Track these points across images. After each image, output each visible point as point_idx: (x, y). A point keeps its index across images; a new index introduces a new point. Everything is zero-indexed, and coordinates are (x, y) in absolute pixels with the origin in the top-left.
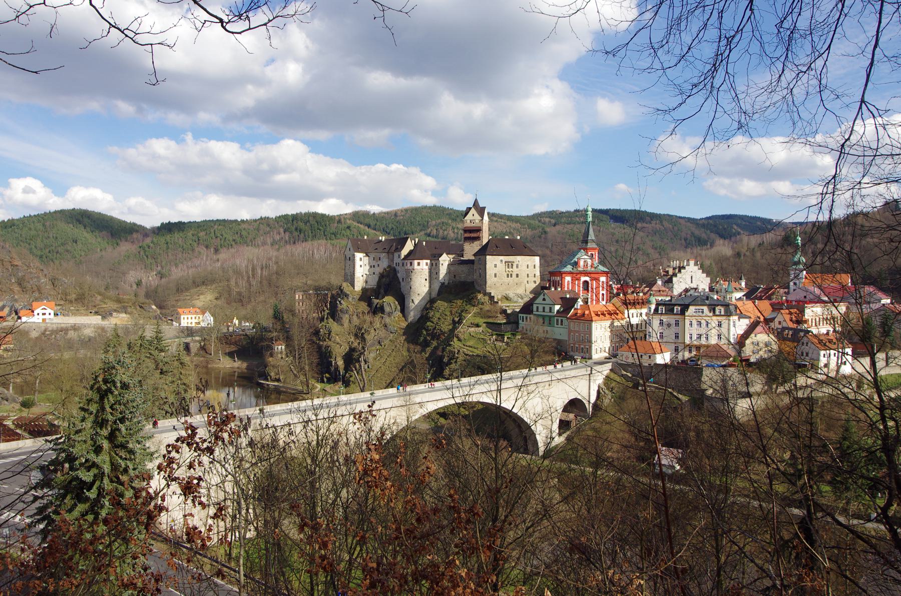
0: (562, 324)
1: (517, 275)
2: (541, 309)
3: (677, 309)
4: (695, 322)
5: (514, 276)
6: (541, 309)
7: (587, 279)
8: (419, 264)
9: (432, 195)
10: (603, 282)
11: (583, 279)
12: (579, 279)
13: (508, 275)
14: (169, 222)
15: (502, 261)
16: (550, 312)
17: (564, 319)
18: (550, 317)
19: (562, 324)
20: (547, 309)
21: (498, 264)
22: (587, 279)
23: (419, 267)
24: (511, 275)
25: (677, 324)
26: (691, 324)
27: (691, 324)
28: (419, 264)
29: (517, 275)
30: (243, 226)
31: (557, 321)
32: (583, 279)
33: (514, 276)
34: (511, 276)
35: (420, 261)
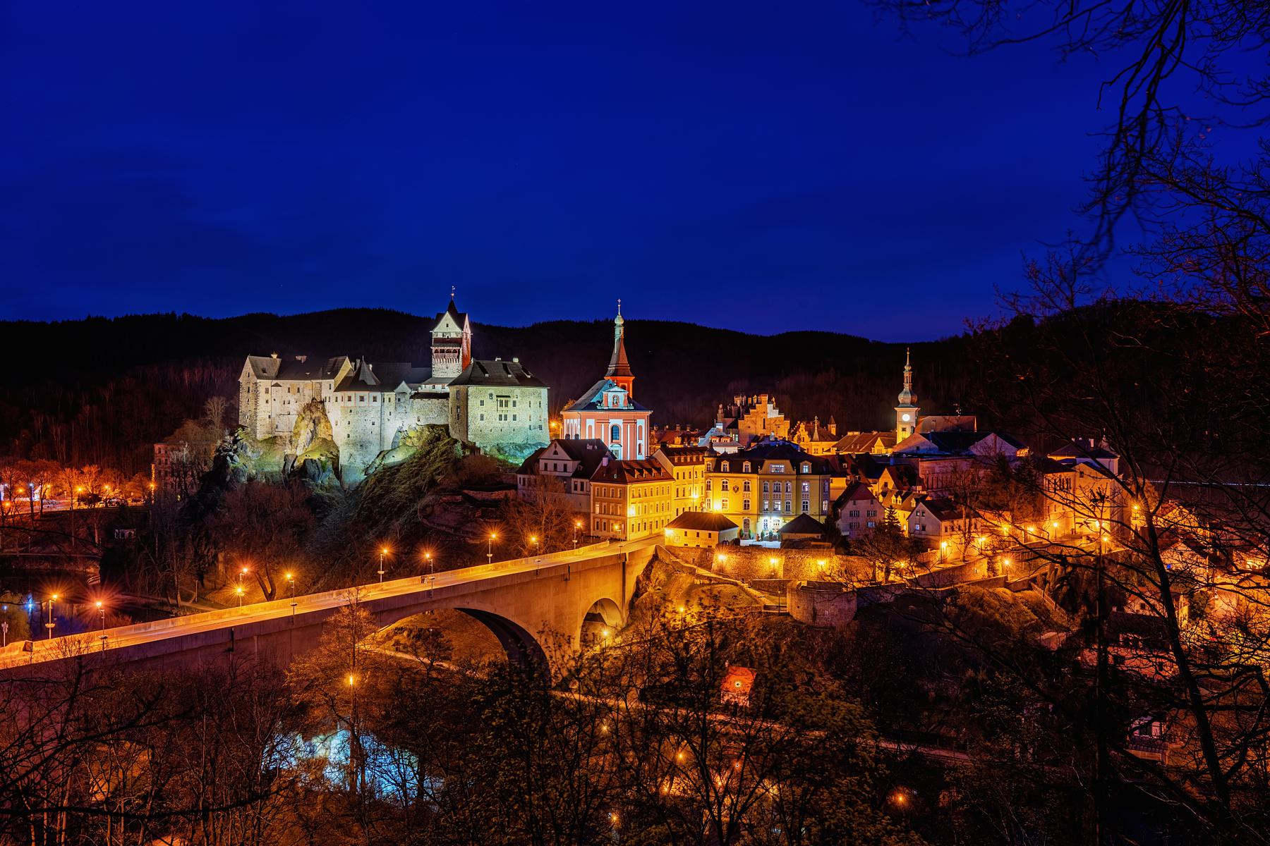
1: (515, 418)
5: (510, 418)
7: (619, 422)
11: (613, 422)
13: (500, 416)
15: (491, 395)
22: (619, 422)
24: (506, 416)
29: (515, 418)
33: (510, 418)
34: (506, 419)
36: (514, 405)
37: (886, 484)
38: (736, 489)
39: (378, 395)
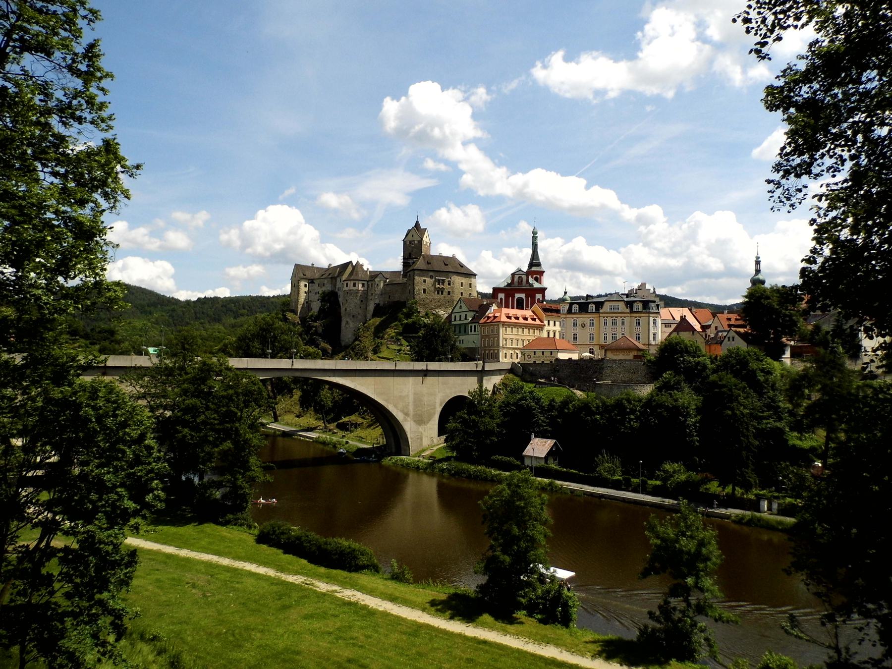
0: (475, 331)
1: (449, 293)
2: (458, 319)
3: (592, 307)
4: (609, 321)
5: (445, 293)
6: (458, 319)
7: (523, 296)
9: (797, 572)
10: (755, 506)
12: (513, 297)
14: (205, 297)
16: (466, 319)
17: (477, 324)
18: (466, 325)
19: (475, 331)
20: (463, 318)
25: (592, 324)
26: (605, 324)
27: (605, 324)
29: (449, 293)
30: (273, 300)
31: (471, 327)
32: (517, 296)
34: (442, 294)
36: (449, 284)
37: (716, 328)
38: (583, 326)
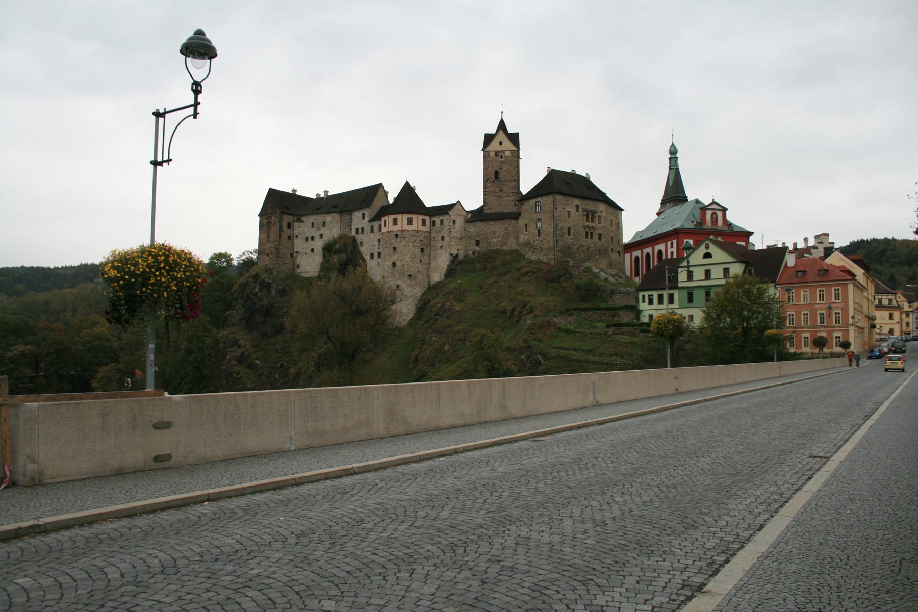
5: (596, 237)
8: (395, 222)
21: (573, 210)
23: (410, 228)
28: (395, 222)
33: (596, 237)
35: (399, 217)
39: (427, 218)
